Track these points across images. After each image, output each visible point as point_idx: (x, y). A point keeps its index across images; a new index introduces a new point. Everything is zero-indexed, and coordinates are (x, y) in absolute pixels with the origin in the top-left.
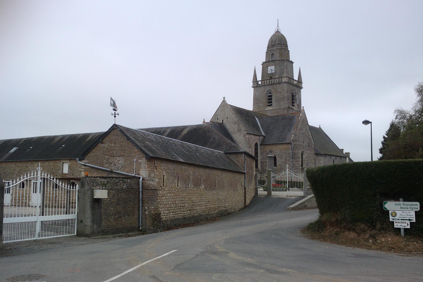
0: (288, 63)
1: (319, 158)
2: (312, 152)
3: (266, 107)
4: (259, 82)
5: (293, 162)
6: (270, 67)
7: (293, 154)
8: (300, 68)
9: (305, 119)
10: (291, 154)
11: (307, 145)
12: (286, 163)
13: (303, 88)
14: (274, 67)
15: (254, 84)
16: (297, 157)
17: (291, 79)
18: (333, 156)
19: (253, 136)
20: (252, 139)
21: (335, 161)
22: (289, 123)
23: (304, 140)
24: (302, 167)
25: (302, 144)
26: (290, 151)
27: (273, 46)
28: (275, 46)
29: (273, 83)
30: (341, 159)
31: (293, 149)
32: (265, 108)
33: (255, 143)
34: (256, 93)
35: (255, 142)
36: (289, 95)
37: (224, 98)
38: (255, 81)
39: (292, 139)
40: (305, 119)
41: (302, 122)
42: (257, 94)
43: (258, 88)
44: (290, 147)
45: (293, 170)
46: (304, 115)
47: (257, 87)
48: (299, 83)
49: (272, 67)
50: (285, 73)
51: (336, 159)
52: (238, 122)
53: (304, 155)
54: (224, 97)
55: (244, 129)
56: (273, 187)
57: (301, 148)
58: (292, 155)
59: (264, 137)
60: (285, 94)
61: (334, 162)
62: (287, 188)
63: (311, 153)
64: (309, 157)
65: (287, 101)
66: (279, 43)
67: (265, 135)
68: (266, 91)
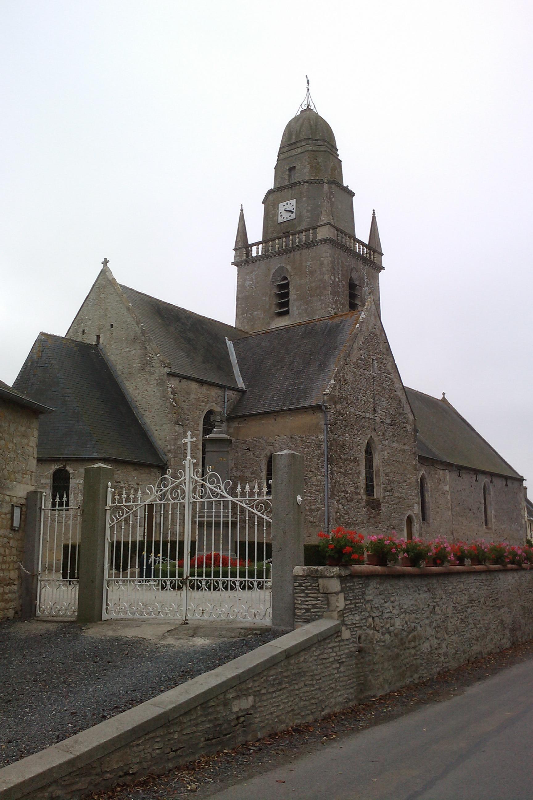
0: (334, 189)
1: (436, 474)
2: (406, 447)
3: (272, 319)
4: (253, 248)
5: (332, 474)
6: (285, 203)
7: (331, 445)
8: (374, 210)
9: (378, 333)
10: (324, 447)
11: (389, 421)
12: (310, 478)
13: (384, 268)
14: (294, 202)
15: (238, 256)
16: (347, 459)
17: (346, 235)
18: (484, 473)
19: (194, 386)
20: (192, 396)
21: (489, 490)
22: (324, 345)
23: (374, 403)
24: (368, 495)
25: (368, 415)
26: (322, 437)
27: (294, 146)
28: (299, 145)
29: (291, 245)
30: (507, 485)
31: (332, 429)
32: (269, 324)
33: (205, 413)
34: (245, 280)
35: (205, 406)
36: (337, 280)
37: (106, 262)
38: (241, 244)
39: (327, 391)
40: (378, 332)
41: (367, 340)
42: (247, 283)
43: (250, 267)
44: (322, 422)
45: (333, 503)
46: (373, 317)
47: (247, 262)
48: (372, 253)
49: (289, 202)
50: (324, 213)
51: (492, 482)
52: (143, 337)
53: (377, 453)
54: (106, 259)
55: (161, 358)
56: (192, 566)
57: (363, 427)
58: (329, 449)
59: (240, 394)
60: (326, 277)
61: (487, 492)
62: (181, 575)
63: (403, 451)
64: (395, 463)
65: (331, 297)
66: (310, 137)
67: (247, 386)
68: (273, 271)
